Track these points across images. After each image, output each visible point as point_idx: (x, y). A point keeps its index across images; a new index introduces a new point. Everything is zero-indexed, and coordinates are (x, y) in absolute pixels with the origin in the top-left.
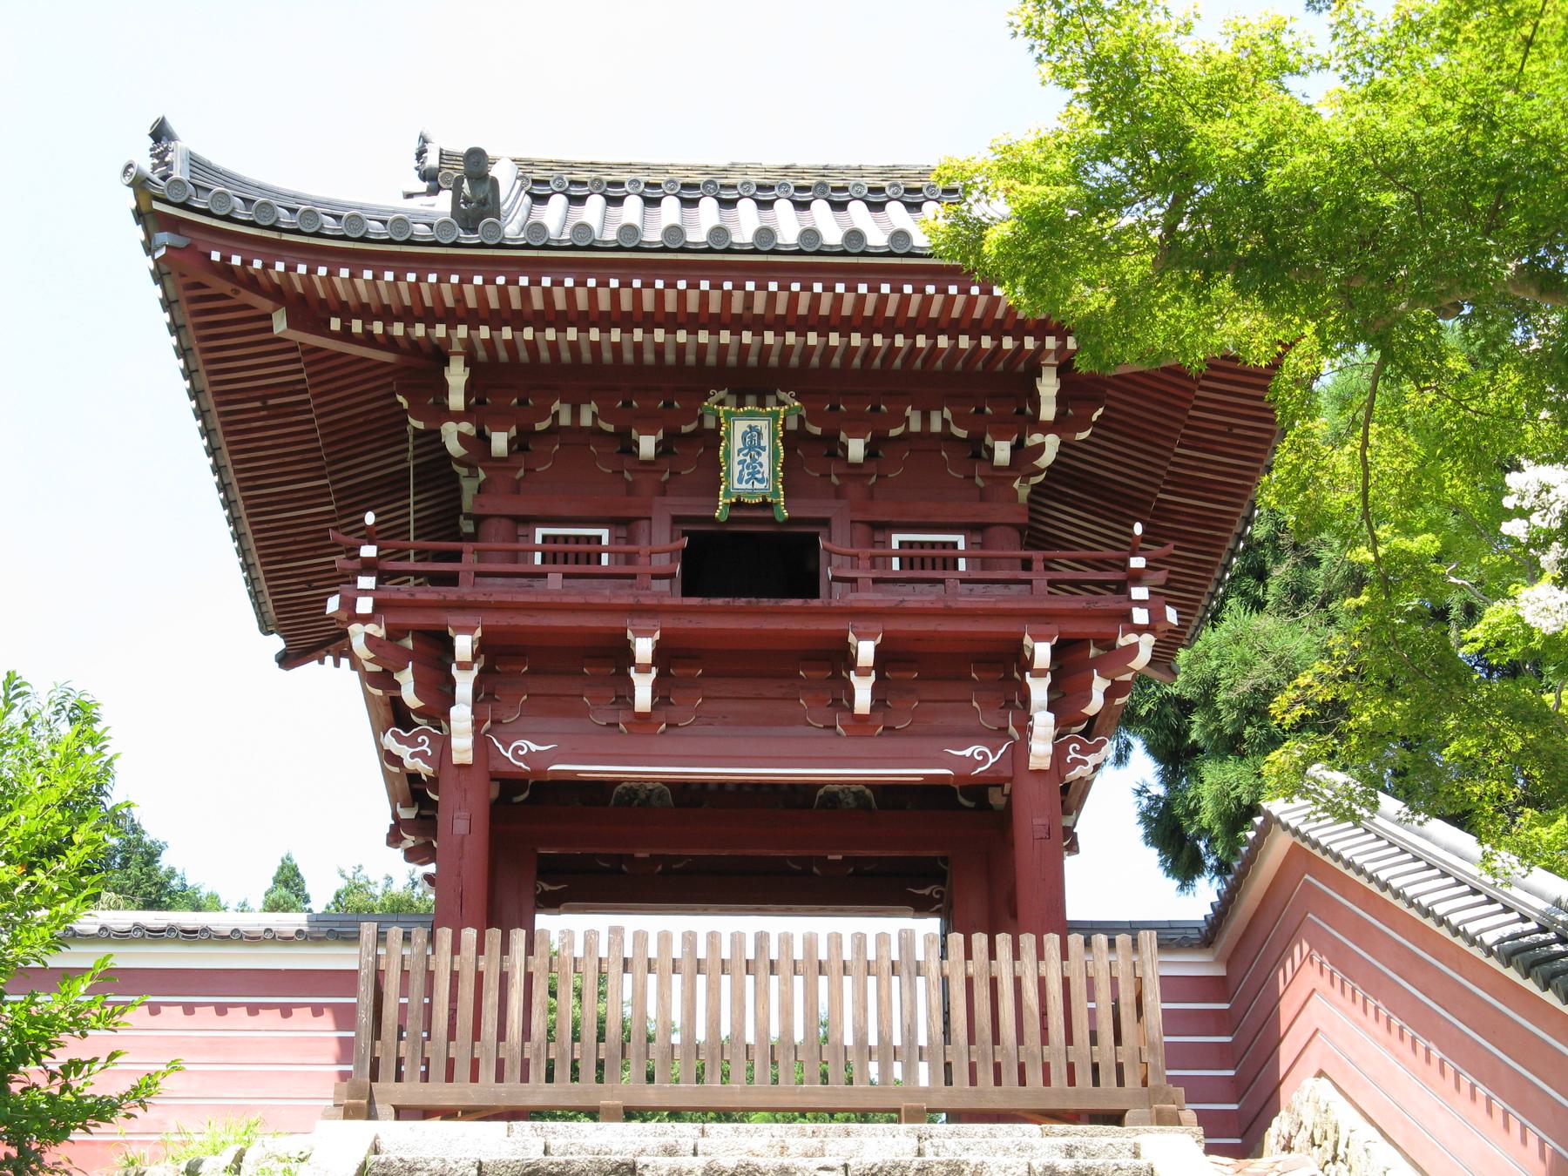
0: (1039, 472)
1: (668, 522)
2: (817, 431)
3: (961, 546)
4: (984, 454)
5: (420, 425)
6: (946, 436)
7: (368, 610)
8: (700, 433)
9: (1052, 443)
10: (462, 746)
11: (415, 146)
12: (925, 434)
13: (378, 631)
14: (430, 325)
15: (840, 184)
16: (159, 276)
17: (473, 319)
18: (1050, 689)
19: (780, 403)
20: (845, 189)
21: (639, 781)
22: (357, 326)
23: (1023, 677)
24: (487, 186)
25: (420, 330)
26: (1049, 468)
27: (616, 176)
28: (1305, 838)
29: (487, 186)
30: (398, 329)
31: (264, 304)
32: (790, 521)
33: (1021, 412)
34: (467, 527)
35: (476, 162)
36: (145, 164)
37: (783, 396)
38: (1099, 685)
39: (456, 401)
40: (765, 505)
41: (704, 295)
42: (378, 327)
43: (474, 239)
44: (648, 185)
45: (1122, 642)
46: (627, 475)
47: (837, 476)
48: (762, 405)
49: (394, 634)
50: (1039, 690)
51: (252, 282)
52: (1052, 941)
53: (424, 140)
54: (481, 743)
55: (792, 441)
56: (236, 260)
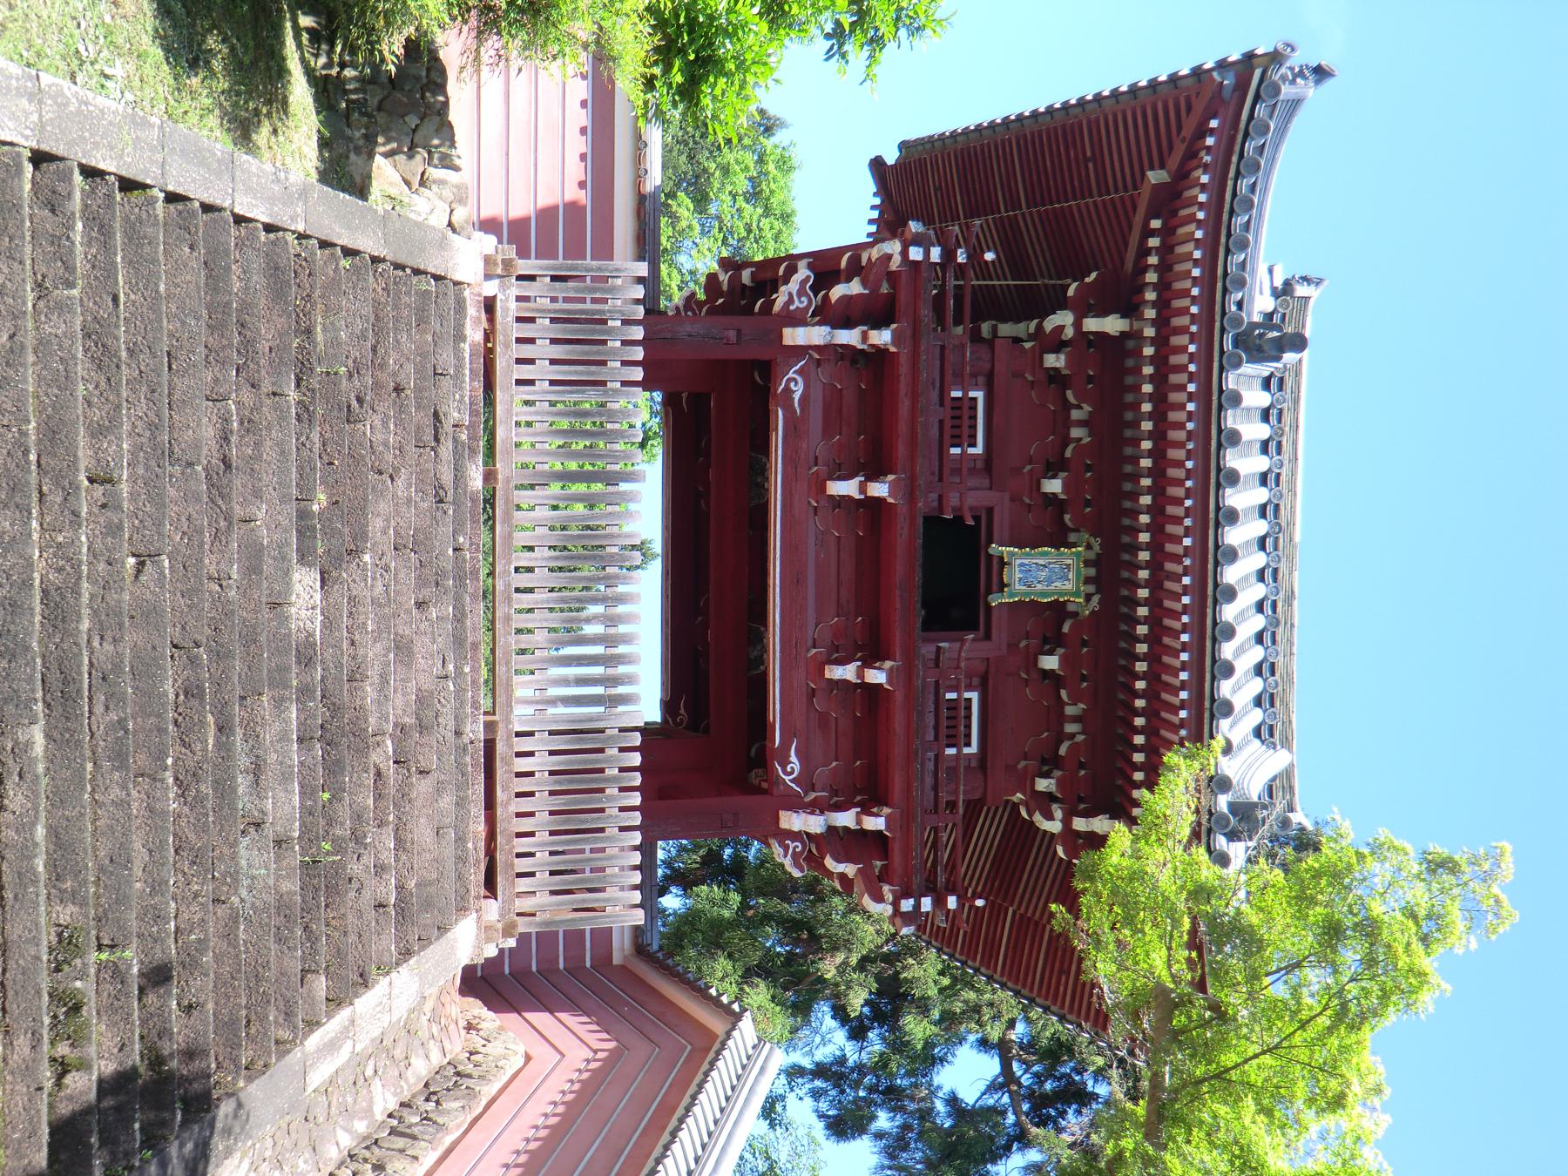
0: (1031, 815)
1: (989, 504)
2: (1066, 628)
3: (966, 750)
4: (1045, 768)
5: (1071, 292)
6: (1061, 737)
7: (912, 257)
8: (1065, 530)
9: (1054, 827)
10: (796, 336)
11: (1312, 274)
12: (1062, 718)
13: (895, 264)
14: (1155, 287)
15: (1278, 638)
16: (1198, 72)
17: (1161, 341)
18: (846, 829)
19: (1088, 597)
20: (1274, 642)
21: (768, 490)
22: (1154, 242)
23: (855, 806)
24: (1274, 353)
25: (1150, 296)
26: (1032, 823)
27: (1287, 418)
28: (723, 1045)
29: (1274, 353)
30: (1151, 277)
31: (1174, 161)
32: (989, 608)
33: (1081, 800)
34: (985, 328)
35: (1299, 343)
36: (1296, 60)
37: (1096, 599)
38: (850, 869)
39: (1091, 324)
40: (1002, 586)
41: (1183, 407)
42: (1153, 260)
43: (1228, 345)
44: (1278, 475)
45: (886, 888)
46: (1029, 467)
47: (1026, 767)
48: (1087, 581)
49: (892, 277)
50: (846, 819)
51: (1192, 154)
52: (636, 838)
53: (1319, 282)
54: (799, 351)
55: (1058, 609)
56: (1210, 141)
